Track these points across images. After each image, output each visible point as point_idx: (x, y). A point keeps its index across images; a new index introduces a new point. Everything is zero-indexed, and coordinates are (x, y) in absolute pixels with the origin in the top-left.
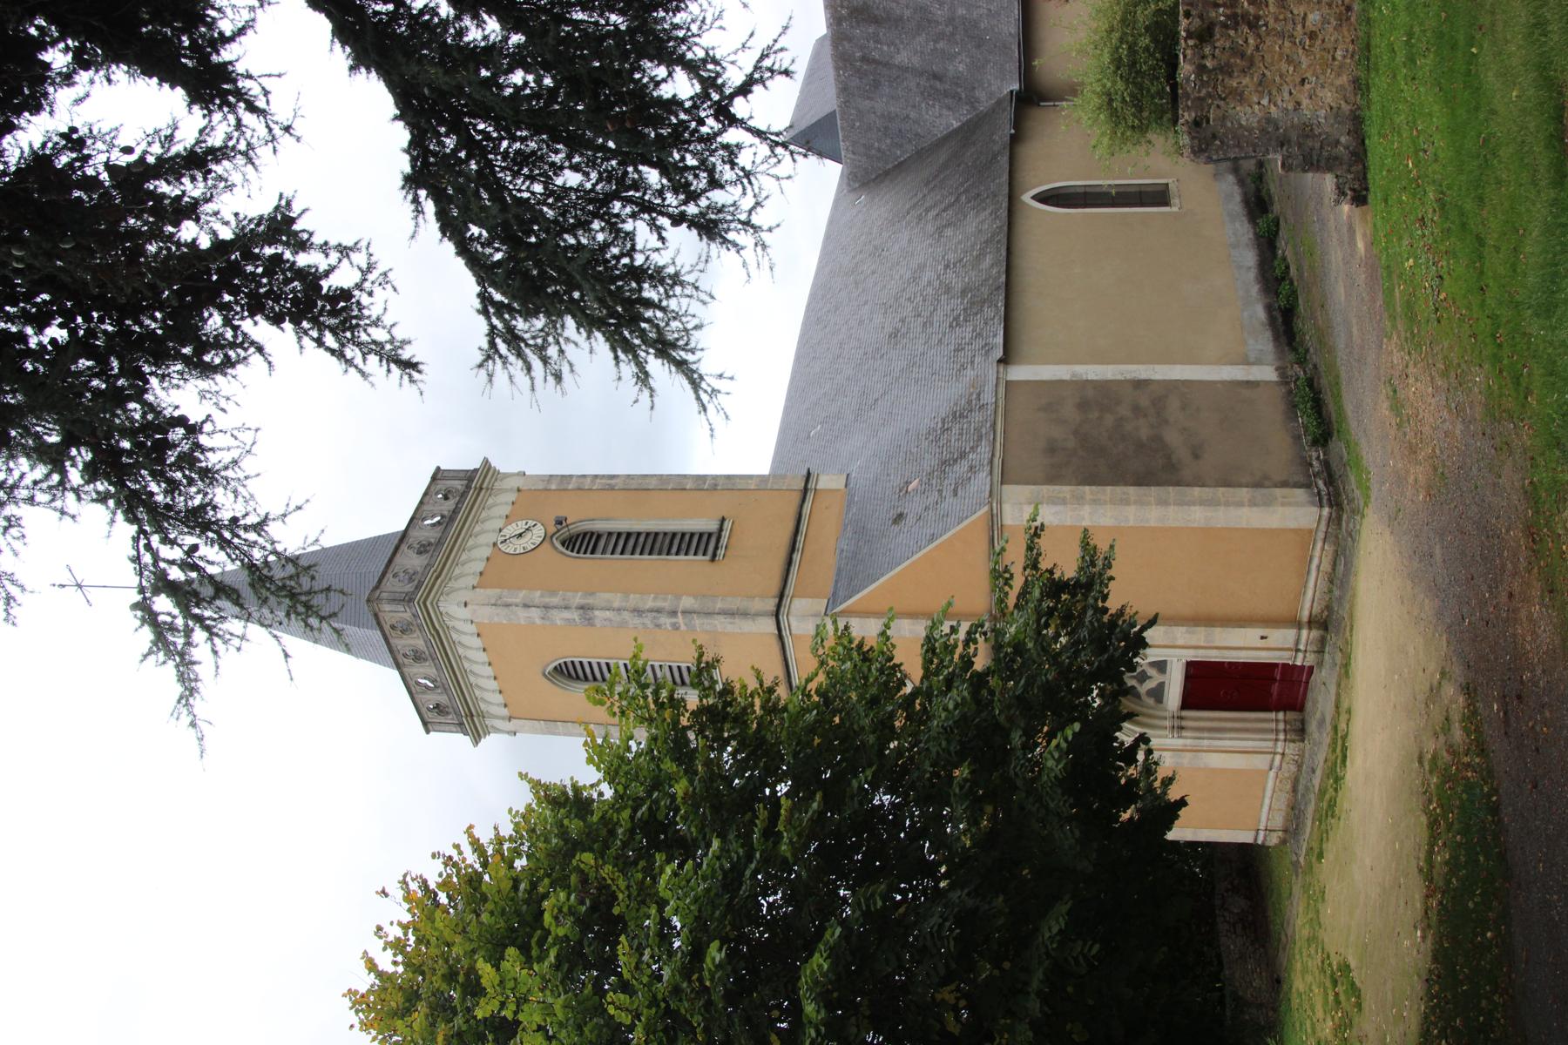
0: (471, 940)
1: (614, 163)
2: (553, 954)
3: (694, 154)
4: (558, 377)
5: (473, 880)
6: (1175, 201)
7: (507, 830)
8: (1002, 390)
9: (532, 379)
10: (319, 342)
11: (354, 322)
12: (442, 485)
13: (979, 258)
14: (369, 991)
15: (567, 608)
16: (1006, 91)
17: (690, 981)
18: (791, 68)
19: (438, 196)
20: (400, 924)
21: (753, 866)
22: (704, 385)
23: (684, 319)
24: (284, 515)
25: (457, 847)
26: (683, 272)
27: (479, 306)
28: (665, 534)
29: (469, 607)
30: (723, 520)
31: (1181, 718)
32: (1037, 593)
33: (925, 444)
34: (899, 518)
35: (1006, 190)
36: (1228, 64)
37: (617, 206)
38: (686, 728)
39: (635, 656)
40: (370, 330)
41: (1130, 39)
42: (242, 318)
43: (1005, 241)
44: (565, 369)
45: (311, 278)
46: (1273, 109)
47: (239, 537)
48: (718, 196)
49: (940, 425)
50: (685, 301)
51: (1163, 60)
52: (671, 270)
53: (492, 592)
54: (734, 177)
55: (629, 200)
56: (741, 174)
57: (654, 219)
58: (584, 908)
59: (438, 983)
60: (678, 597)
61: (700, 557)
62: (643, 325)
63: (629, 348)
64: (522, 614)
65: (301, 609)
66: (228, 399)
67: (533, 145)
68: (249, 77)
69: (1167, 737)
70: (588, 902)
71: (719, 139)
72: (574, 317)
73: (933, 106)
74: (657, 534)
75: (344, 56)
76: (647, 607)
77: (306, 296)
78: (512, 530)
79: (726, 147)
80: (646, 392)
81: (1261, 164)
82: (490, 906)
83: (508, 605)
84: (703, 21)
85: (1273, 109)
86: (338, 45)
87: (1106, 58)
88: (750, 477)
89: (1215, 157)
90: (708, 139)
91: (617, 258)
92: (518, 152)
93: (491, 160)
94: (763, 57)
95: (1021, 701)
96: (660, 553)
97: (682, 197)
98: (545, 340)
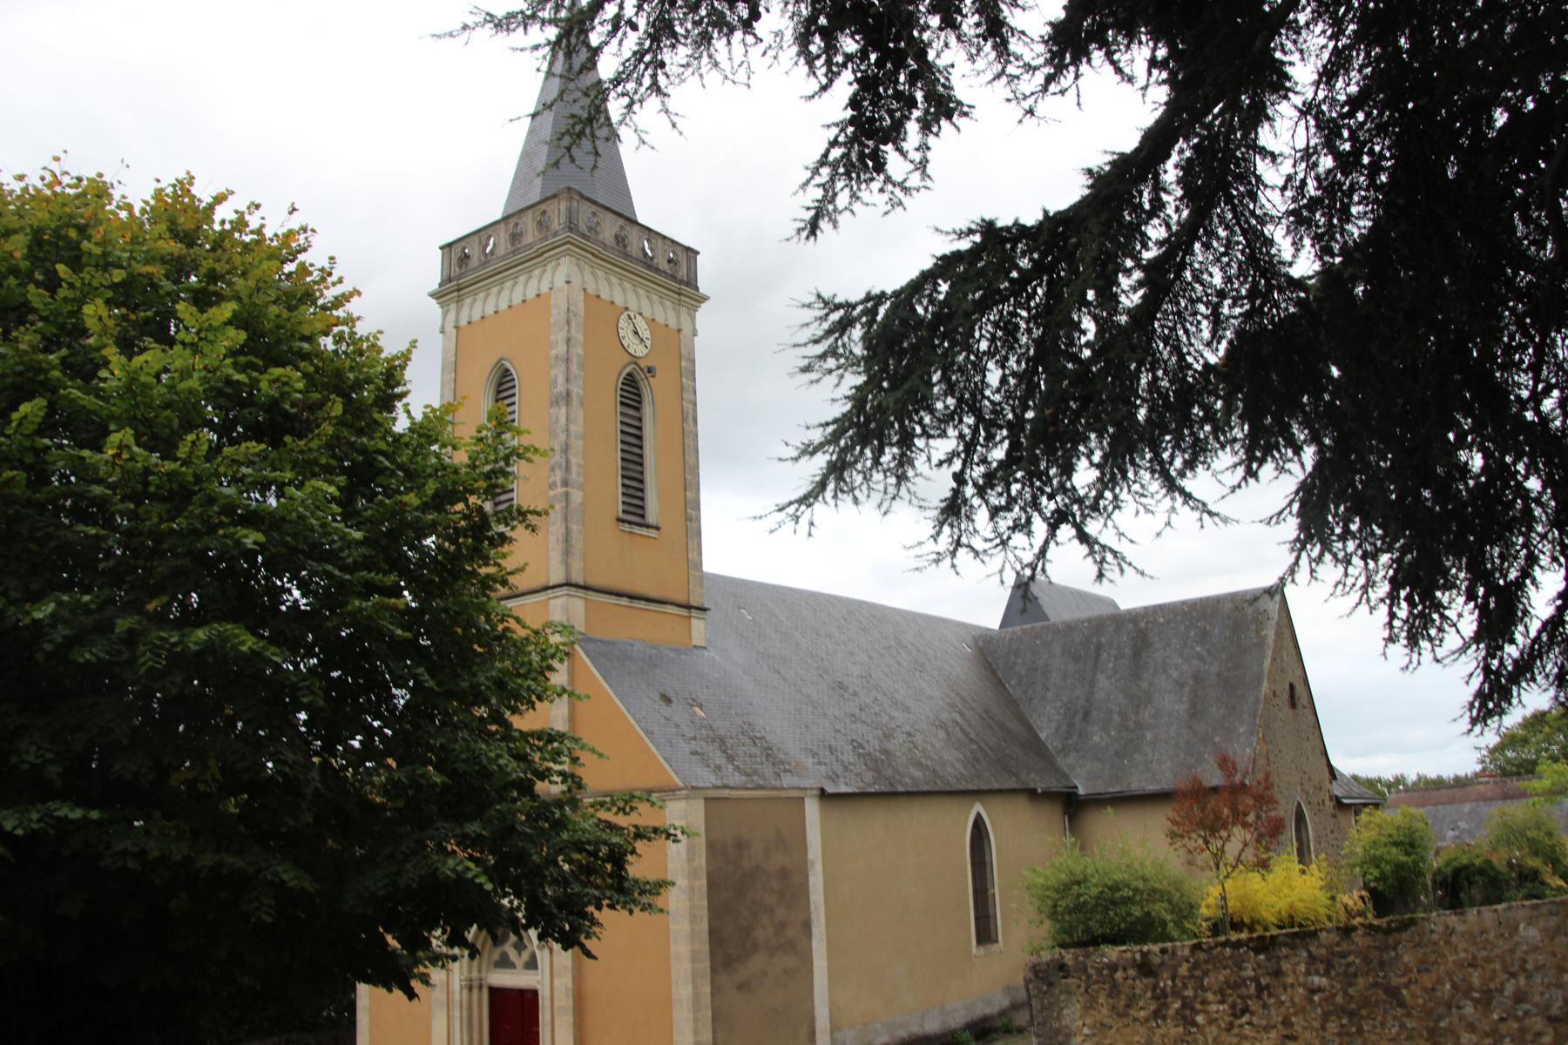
0: (250, 296)
1: (1010, 416)
2: (241, 377)
3: (1020, 493)
4: (807, 369)
5: (308, 297)
6: (982, 950)
7: (361, 329)
8: (794, 793)
9: (805, 345)
10: (834, 143)
11: (854, 175)
12: (682, 257)
13: (919, 765)
14: (194, 197)
15: (568, 380)
16: (1076, 782)
17: (220, 514)
18: (1105, 580)
19: (975, 252)
20: (263, 226)
21: (337, 572)
22: (803, 508)
23: (864, 487)
24: (667, 111)
25: (340, 281)
26: (909, 484)
27: (873, 293)
28: (642, 473)
29: (566, 286)
30: (657, 528)
31: (480, 987)
32: (615, 840)
33: (739, 721)
34: (667, 700)
35: (984, 787)
36: (1119, 992)
37: (969, 420)
38: (466, 501)
39: (536, 450)
40: (847, 191)
41: (1138, 898)
42: (854, 72)
43: (937, 789)
44: (813, 376)
45: (894, 134)
46: (1079, 1039)
47: (646, 69)
48: (982, 515)
49: (758, 735)
50: (881, 487)
51: (1120, 930)
52: (910, 473)
53: (580, 308)
54: (1002, 530)
55: (975, 431)
56: (1005, 537)
57: (959, 455)
58: (287, 407)
59: (207, 264)
60: (581, 487)
61: (621, 507)
62: (858, 448)
63: (834, 439)
64: (559, 337)
65: (578, 128)
66: (775, 58)
67: (1024, 340)
68: (1077, 77)
69: (461, 973)
70: (294, 411)
71: (1036, 514)
72: (866, 383)
73: (1059, 713)
74: (641, 464)
75: (1100, 163)
76: (571, 458)
77: (878, 130)
78: (642, 325)
79: (1029, 521)
80: (795, 454)
81: (1021, 1030)
82: (286, 314)
83: (568, 323)
84: (1142, 495)
85: (1079, 1039)
86: (1109, 158)
87: (1118, 876)
88: (700, 553)
89: (1031, 986)
90: (1035, 505)
91: (920, 422)
92: (1017, 326)
93: (1008, 301)
94: (1115, 553)
95: (511, 830)
96: (623, 468)
97: (981, 482)
98: (841, 356)
